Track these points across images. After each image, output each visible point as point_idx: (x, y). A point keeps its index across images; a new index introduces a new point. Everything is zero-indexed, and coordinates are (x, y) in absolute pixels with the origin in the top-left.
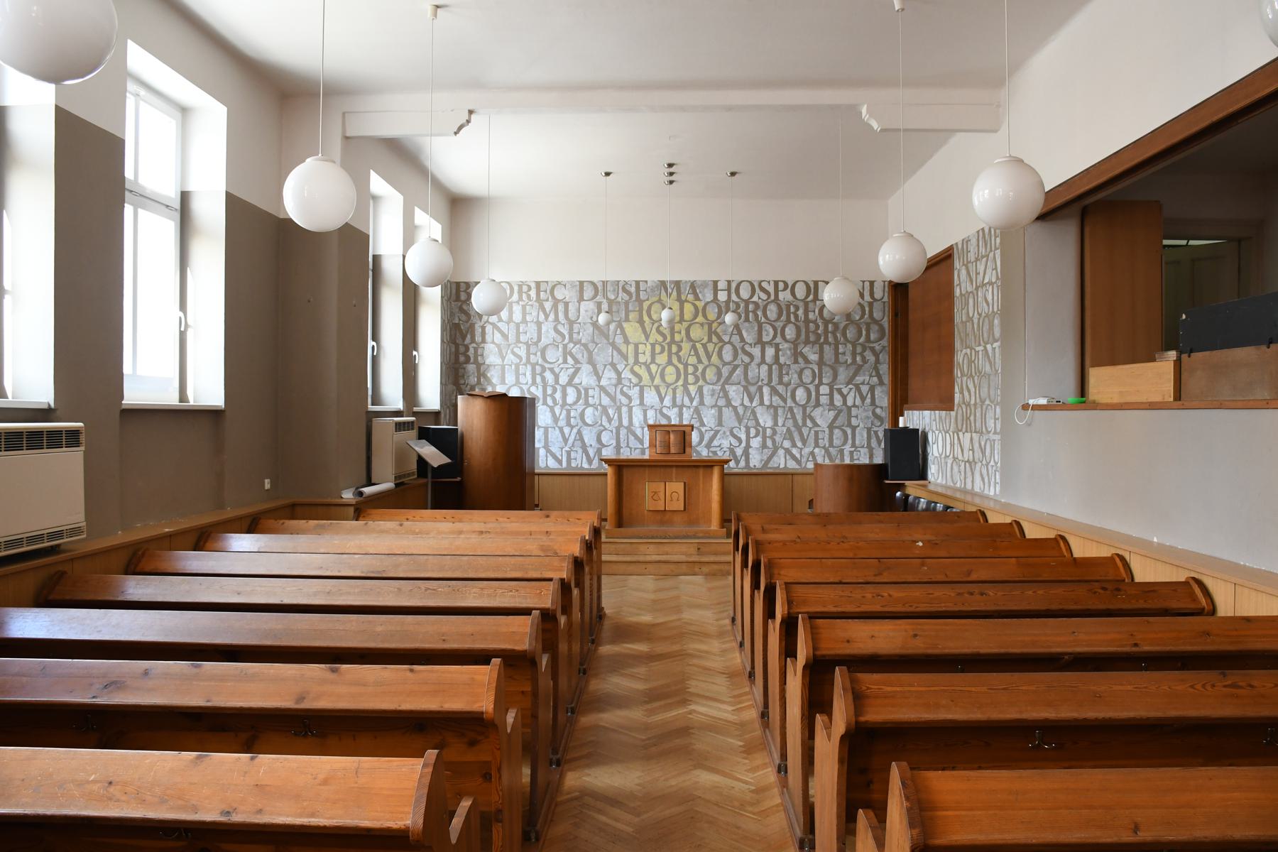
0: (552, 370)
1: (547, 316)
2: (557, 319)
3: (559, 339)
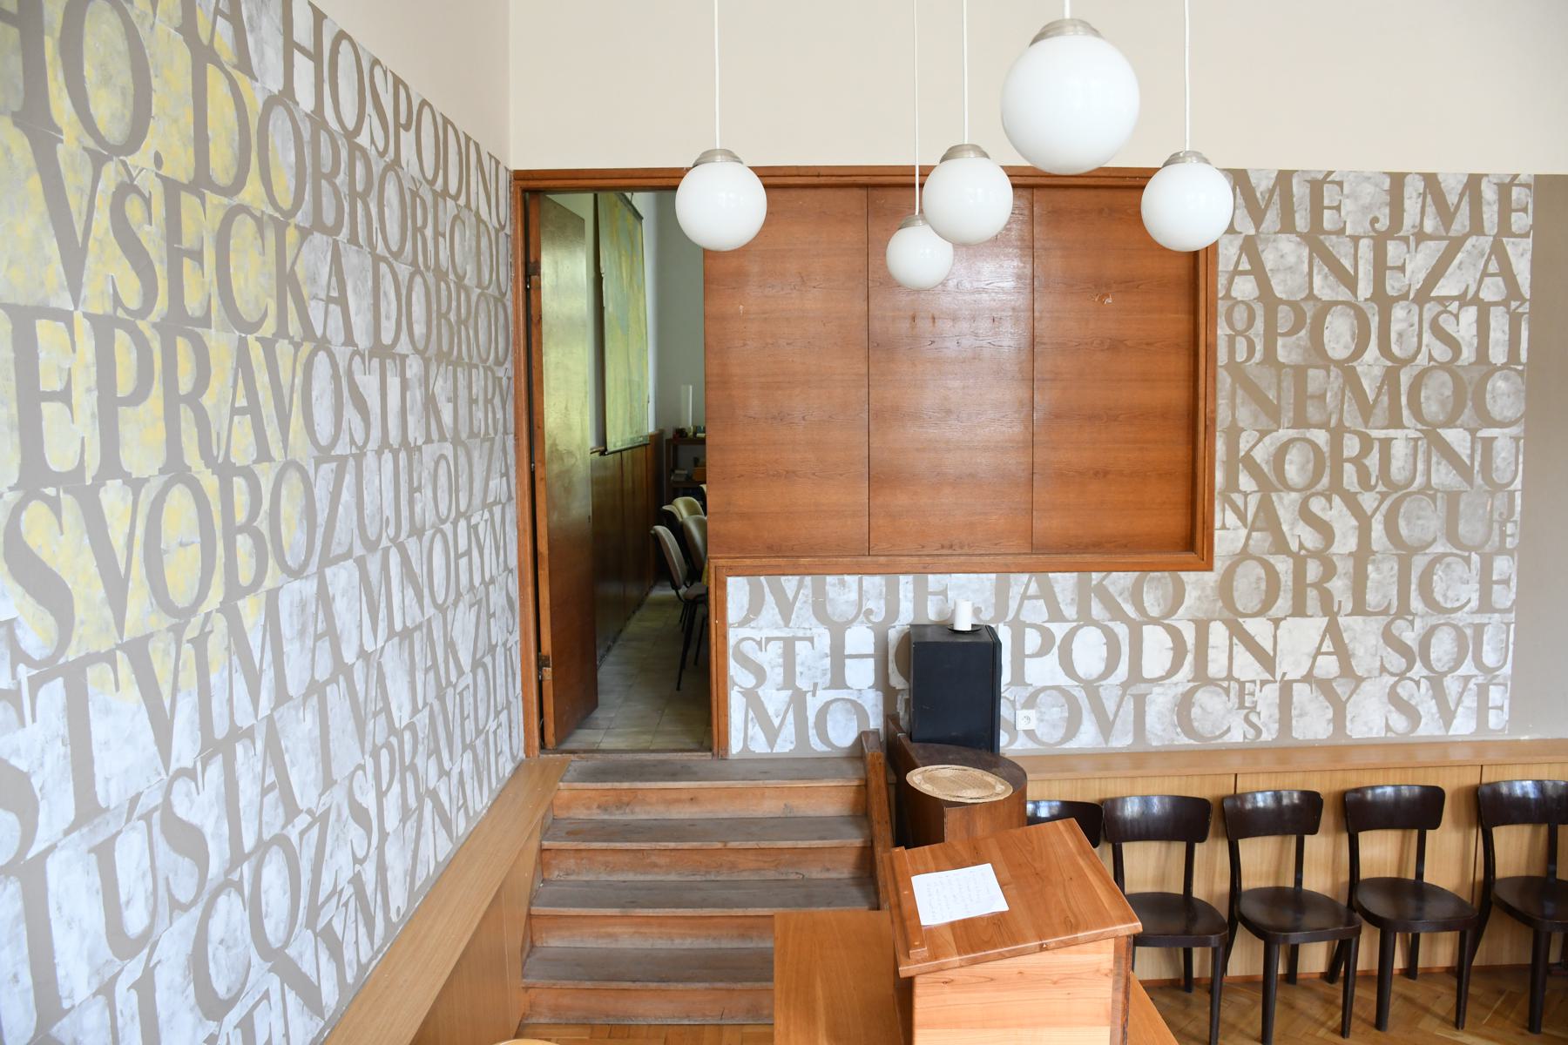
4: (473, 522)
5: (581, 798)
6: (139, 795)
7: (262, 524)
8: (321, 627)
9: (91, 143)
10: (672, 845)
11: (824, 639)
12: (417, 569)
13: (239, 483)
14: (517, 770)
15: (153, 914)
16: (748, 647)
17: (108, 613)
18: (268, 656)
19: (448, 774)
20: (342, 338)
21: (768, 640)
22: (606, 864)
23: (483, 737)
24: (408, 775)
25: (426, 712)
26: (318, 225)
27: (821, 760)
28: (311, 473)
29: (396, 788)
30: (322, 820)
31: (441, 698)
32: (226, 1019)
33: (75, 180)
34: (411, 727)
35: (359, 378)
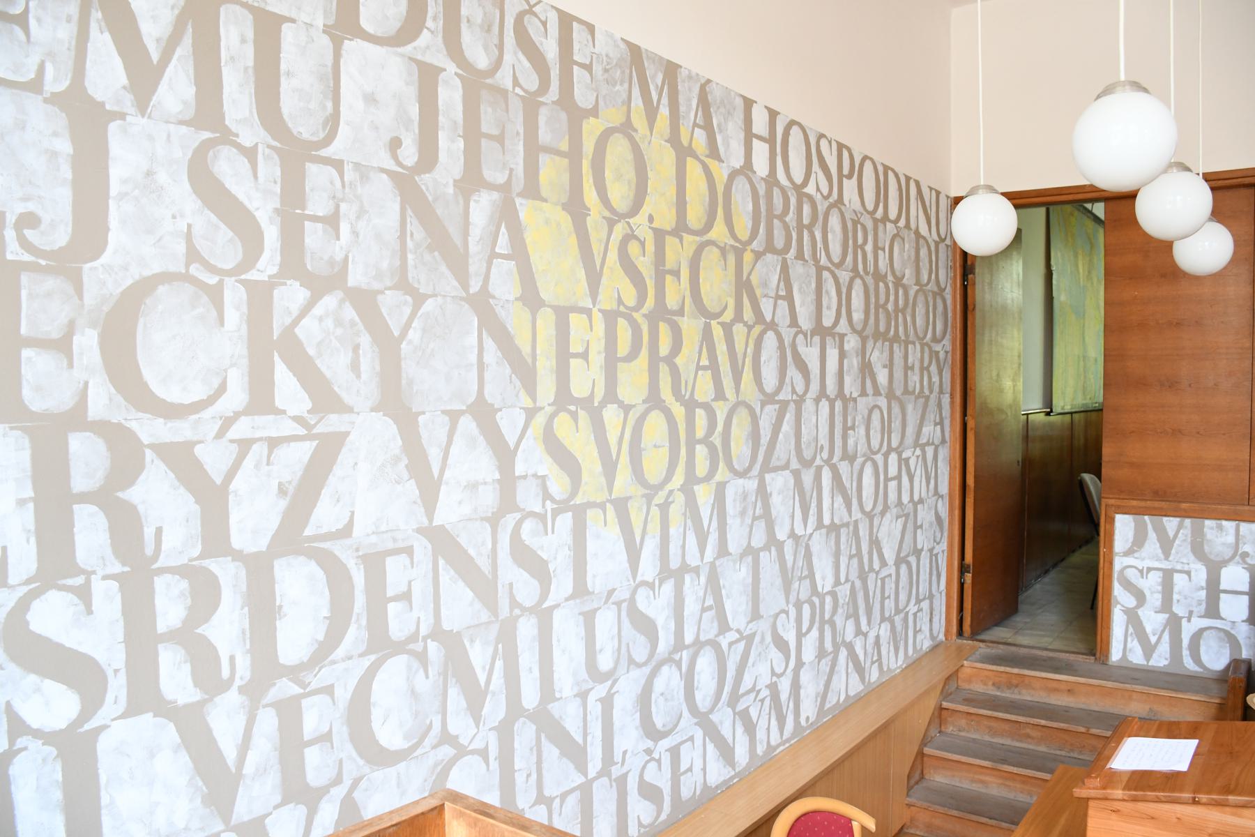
0: (181, 460)
1: (144, 77)
2: (207, 109)
3: (222, 246)
4: (904, 456)
5: (979, 674)
6: (614, 590)
7: (716, 439)
8: (758, 512)
9: (607, 214)
10: (1043, 722)
11: (1200, 574)
12: (848, 485)
13: (700, 414)
14: (934, 648)
15: (617, 662)
16: (1131, 574)
17: (603, 480)
18: (715, 524)
19: (865, 635)
20: (788, 321)
21: (1149, 569)
22: (990, 728)
23: (902, 615)
24: (827, 627)
25: (848, 586)
26: (770, 248)
27: (1192, 677)
28: (758, 410)
29: (815, 633)
30: (750, 639)
31: (863, 577)
32: (661, 743)
33: (597, 233)
34: (833, 594)
35: (802, 349)
